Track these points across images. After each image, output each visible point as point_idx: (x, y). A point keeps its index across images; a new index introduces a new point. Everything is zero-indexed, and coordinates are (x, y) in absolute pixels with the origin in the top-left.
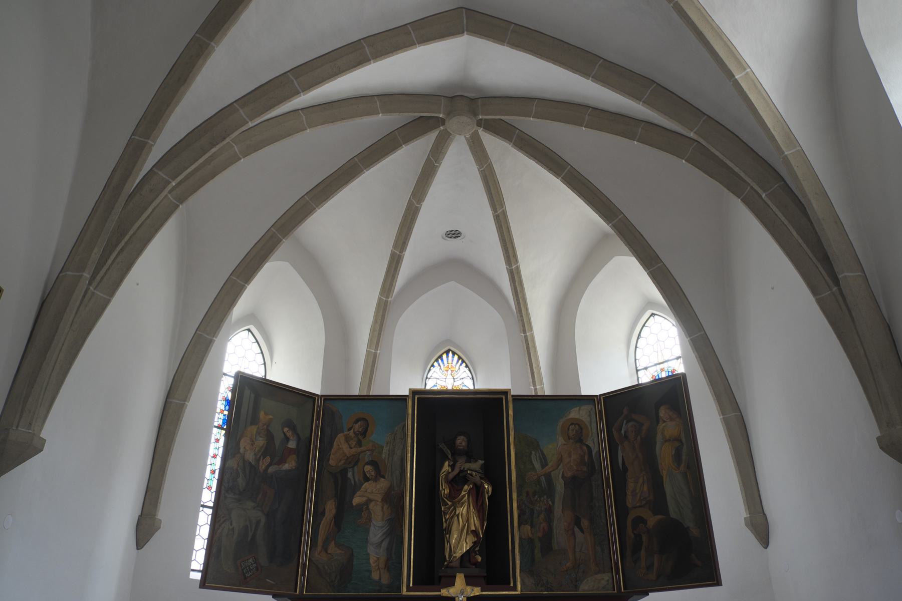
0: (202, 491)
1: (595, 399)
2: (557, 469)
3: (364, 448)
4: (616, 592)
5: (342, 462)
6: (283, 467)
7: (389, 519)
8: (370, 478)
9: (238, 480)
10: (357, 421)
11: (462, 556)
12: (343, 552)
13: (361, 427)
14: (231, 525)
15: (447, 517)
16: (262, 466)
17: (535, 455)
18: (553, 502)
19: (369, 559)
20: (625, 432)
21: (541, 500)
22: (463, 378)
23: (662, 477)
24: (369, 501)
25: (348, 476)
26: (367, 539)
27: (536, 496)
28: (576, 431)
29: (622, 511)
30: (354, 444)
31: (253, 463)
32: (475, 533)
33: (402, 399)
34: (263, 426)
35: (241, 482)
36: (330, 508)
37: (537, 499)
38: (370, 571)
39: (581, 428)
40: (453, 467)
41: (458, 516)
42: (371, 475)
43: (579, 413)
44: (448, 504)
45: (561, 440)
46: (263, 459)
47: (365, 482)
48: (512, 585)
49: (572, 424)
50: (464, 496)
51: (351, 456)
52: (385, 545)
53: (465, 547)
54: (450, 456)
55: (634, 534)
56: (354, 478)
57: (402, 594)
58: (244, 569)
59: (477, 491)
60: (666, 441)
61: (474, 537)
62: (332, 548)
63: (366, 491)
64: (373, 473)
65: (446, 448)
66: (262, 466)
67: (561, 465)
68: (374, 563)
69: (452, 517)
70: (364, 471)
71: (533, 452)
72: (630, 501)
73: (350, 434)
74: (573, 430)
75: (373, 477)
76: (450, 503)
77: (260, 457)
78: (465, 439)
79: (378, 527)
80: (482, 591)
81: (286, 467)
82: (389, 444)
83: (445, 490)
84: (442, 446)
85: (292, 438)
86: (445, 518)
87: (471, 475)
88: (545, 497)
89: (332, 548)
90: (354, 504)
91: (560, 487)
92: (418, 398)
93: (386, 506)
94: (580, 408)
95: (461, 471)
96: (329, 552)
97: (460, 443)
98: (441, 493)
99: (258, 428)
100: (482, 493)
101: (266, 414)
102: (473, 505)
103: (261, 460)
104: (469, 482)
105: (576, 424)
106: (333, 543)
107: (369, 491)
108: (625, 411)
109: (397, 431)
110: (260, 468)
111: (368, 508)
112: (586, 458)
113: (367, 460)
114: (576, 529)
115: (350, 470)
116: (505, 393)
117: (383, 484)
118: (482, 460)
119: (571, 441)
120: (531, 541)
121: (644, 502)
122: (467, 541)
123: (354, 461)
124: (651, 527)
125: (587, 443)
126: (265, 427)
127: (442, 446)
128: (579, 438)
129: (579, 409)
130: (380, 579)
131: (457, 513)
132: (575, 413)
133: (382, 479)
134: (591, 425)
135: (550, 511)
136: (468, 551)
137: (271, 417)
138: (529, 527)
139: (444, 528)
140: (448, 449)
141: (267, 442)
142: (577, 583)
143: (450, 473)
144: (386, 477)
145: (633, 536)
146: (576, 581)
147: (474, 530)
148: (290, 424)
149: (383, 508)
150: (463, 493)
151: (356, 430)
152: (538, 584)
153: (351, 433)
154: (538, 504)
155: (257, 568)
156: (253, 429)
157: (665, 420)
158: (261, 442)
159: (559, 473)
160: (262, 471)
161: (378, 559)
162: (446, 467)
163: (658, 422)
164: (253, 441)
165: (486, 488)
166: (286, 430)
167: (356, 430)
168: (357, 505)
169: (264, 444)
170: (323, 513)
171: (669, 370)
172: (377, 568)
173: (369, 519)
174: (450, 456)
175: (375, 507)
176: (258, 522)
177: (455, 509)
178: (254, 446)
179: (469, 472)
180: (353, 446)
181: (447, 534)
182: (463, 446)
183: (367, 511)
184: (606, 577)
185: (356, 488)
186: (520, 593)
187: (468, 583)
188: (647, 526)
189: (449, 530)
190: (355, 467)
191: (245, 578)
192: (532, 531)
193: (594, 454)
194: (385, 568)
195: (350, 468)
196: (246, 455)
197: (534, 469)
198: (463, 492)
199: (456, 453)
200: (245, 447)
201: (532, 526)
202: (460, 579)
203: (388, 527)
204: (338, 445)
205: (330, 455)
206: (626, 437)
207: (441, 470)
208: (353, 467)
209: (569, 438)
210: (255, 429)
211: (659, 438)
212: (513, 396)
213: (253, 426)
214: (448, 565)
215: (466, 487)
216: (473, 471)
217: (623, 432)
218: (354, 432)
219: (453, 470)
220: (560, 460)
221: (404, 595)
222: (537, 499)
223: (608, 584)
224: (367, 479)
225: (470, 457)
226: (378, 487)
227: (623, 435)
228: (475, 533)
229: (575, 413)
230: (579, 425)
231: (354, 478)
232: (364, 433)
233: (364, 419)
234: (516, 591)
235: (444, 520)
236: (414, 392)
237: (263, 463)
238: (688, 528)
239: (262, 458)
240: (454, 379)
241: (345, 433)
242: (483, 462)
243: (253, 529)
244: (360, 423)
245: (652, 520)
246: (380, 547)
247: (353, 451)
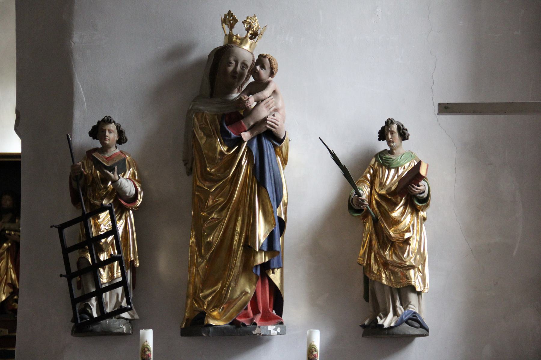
87: (10, 234)
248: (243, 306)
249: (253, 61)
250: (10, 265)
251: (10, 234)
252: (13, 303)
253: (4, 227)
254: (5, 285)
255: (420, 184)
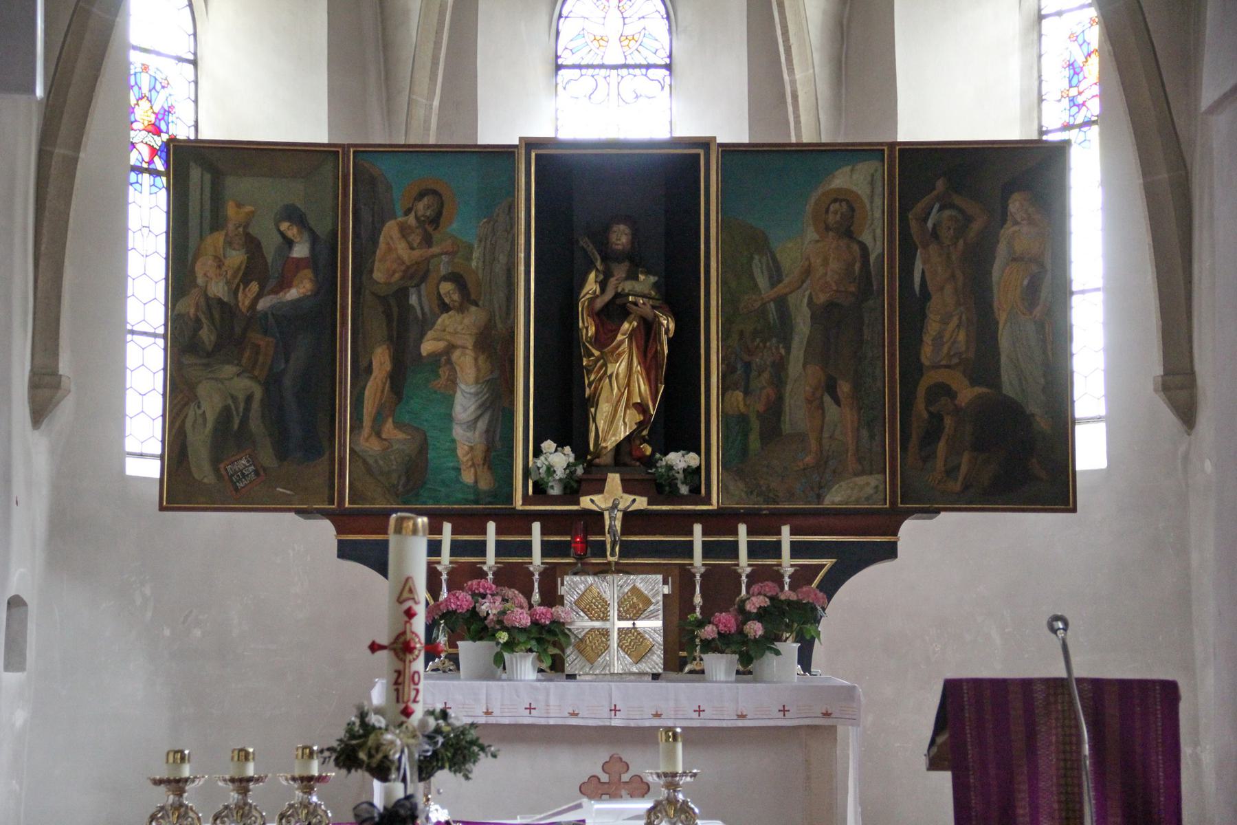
0: (125, 394)
1: (883, 150)
2: (800, 287)
3: (435, 250)
4: (888, 506)
5: (397, 276)
6: (288, 295)
7: (488, 381)
8: (451, 306)
9: (200, 332)
10: (421, 196)
11: (619, 446)
12: (409, 437)
13: (428, 208)
14: (199, 407)
15: (592, 378)
16: (244, 301)
17: (760, 261)
18: (788, 349)
19: (454, 450)
20: (934, 225)
21: (765, 347)
22: (643, 17)
23: (997, 323)
24: (451, 347)
25: (410, 302)
26: (450, 415)
27: (758, 340)
28: (842, 214)
29: (911, 369)
30: (418, 241)
31: (225, 300)
32: (641, 408)
33: (504, 154)
34: (237, 229)
35: (207, 335)
36: (381, 360)
37: (759, 344)
38: (458, 470)
39: (852, 209)
40: (603, 285)
41: (611, 377)
42: (453, 301)
43: (851, 177)
44: (593, 355)
45: (811, 234)
46: (244, 289)
47: (442, 313)
49: (835, 200)
50: (622, 342)
51: (413, 265)
52: (482, 425)
53: (622, 433)
55: (930, 413)
56: (422, 309)
57: (514, 508)
58: (232, 475)
59: (648, 329)
60: (1014, 260)
61: (639, 413)
62: (389, 427)
63: (444, 330)
64: (456, 297)
65: (591, 246)
66: (244, 301)
67: (808, 282)
68: (464, 456)
69: (601, 379)
70: (439, 293)
72: (927, 353)
73: (409, 223)
74: (836, 213)
75: (456, 304)
76: (597, 353)
77: (238, 286)
78: (627, 231)
79: (470, 393)
80: (649, 504)
81: (293, 294)
82: (483, 243)
83: (588, 328)
84: (585, 242)
85: (298, 240)
86: (589, 379)
87: (635, 304)
88: (774, 340)
89: (389, 427)
90: (424, 353)
91: (803, 326)
92: (536, 155)
93: (482, 359)
94: (854, 166)
95: (617, 295)
96: (384, 436)
98: (582, 333)
99: (226, 235)
100: (655, 334)
101: (239, 205)
102: (637, 358)
103: (241, 290)
104: (633, 316)
105: (844, 200)
106: (390, 420)
107: (450, 329)
108: (940, 185)
110: (240, 304)
111: (449, 362)
112: (857, 267)
113: (443, 271)
114: (827, 399)
115: (412, 290)
116: (705, 144)
117: (474, 317)
118: (654, 275)
119: (831, 233)
120: (743, 419)
121: (955, 361)
122: (626, 420)
123: (418, 274)
124: (963, 404)
125: (860, 239)
126: (241, 229)
127: (585, 242)
128: (847, 231)
129: (852, 170)
130: (476, 482)
131: (609, 373)
132: (844, 179)
133: (473, 309)
134: (872, 202)
135: (780, 367)
136: (628, 439)
137: (249, 208)
138: (741, 394)
139: (586, 396)
140: (594, 251)
141: (247, 257)
142: (821, 492)
143: (597, 296)
144: (481, 303)
145: (925, 415)
146: (821, 487)
147: (639, 403)
148: (293, 215)
149: (476, 359)
150: (620, 337)
151: (420, 213)
152: (752, 493)
153: (411, 220)
154: (761, 354)
155: (257, 473)
156: (217, 240)
157: (1019, 220)
158: (236, 258)
159: (804, 296)
160: (244, 310)
161: (471, 448)
162: (591, 285)
163: (1004, 221)
164: (220, 261)
165: (662, 324)
166: (284, 226)
167: (420, 213)
168: (429, 355)
169: (241, 263)
170: (369, 370)
172: (470, 463)
173: (453, 382)
175: (462, 358)
176: (249, 399)
177: (605, 365)
178: (224, 269)
179: (631, 298)
180: (415, 245)
181: (592, 407)
182: (623, 244)
183: (448, 366)
184: (873, 480)
185: (426, 325)
186: (716, 508)
187: (626, 490)
188: (956, 402)
189: (593, 401)
190: (423, 286)
191: (237, 489)
193: (872, 258)
194: (484, 464)
195: (412, 287)
196: (209, 288)
197: (755, 287)
198: (619, 335)
199: (609, 257)
200: (205, 274)
201: (747, 393)
202: (614, 479)
203: (487, 395)
204: (388, 244)
205: (373, 262)
206: (935, 234)
207: (580, 293)
208: (418, 286)
209: (827, 228)
210: (221, 240)
211: (1002, 250)
213: (216, 234)
214: (591, 460)
215: (626, 326)
216: (640, 296)
217: (930, 224)
218: (417, 218)
219: (603, 290)
220: (808, 272)
221: (519, 510)
222: (759, 344)
223: (876, 493)
224: (445, 308)
225: (636, 261)
226: (466, 321)
227: (930, 229)
228: (641, 408)
229: (844, 179)
230: (848, 202)
231: (422, 309)
232: (436, 220)
233: (434, 192)
234: (710, 504)
235: (586, 382)
236: (530, 144)
237: (246, 296)
238: (1033, 415)
239: (242, 287)
240: (624, 18)
241: (400, 219)
242: (656, 278)
243: (241, 409)
244: (426, 199)
245: (967, 394)
246: (475, 428)
247: (417, 254)
248: (404, 587)
249: (819, 639)
250: (637, 367)
251: (635, 304)
252: (641, 444)
253: (623, 289)
254: (627, 407)
255: (483, 614)
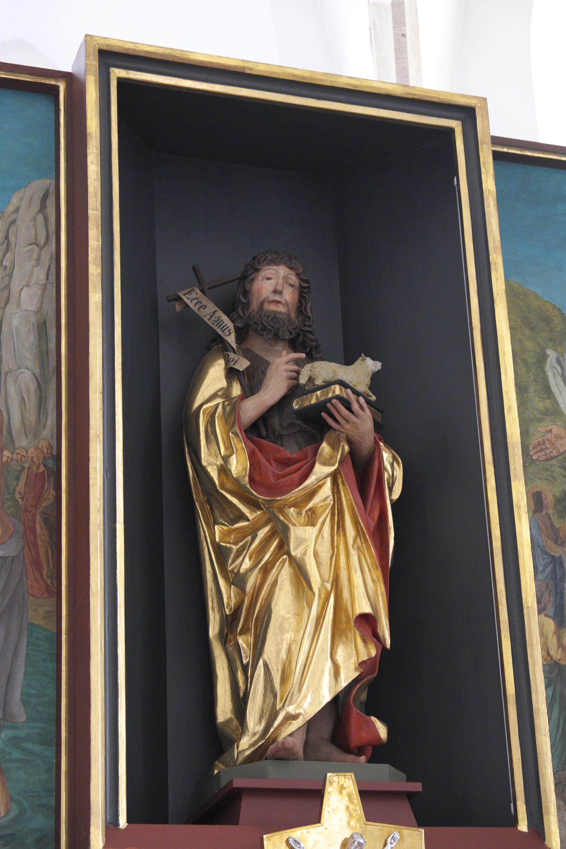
44: (242, 517)
48: (523, 826)
54: (231, 339)
71: (549, 352)
78: (294, 279)
87: (347, 405)
97: (275, 292)
109: (17, 210)
171: (235, 359)
174: (231, 339)
182: (286, 304)
192: (559, 639)
212: (496, 140)
